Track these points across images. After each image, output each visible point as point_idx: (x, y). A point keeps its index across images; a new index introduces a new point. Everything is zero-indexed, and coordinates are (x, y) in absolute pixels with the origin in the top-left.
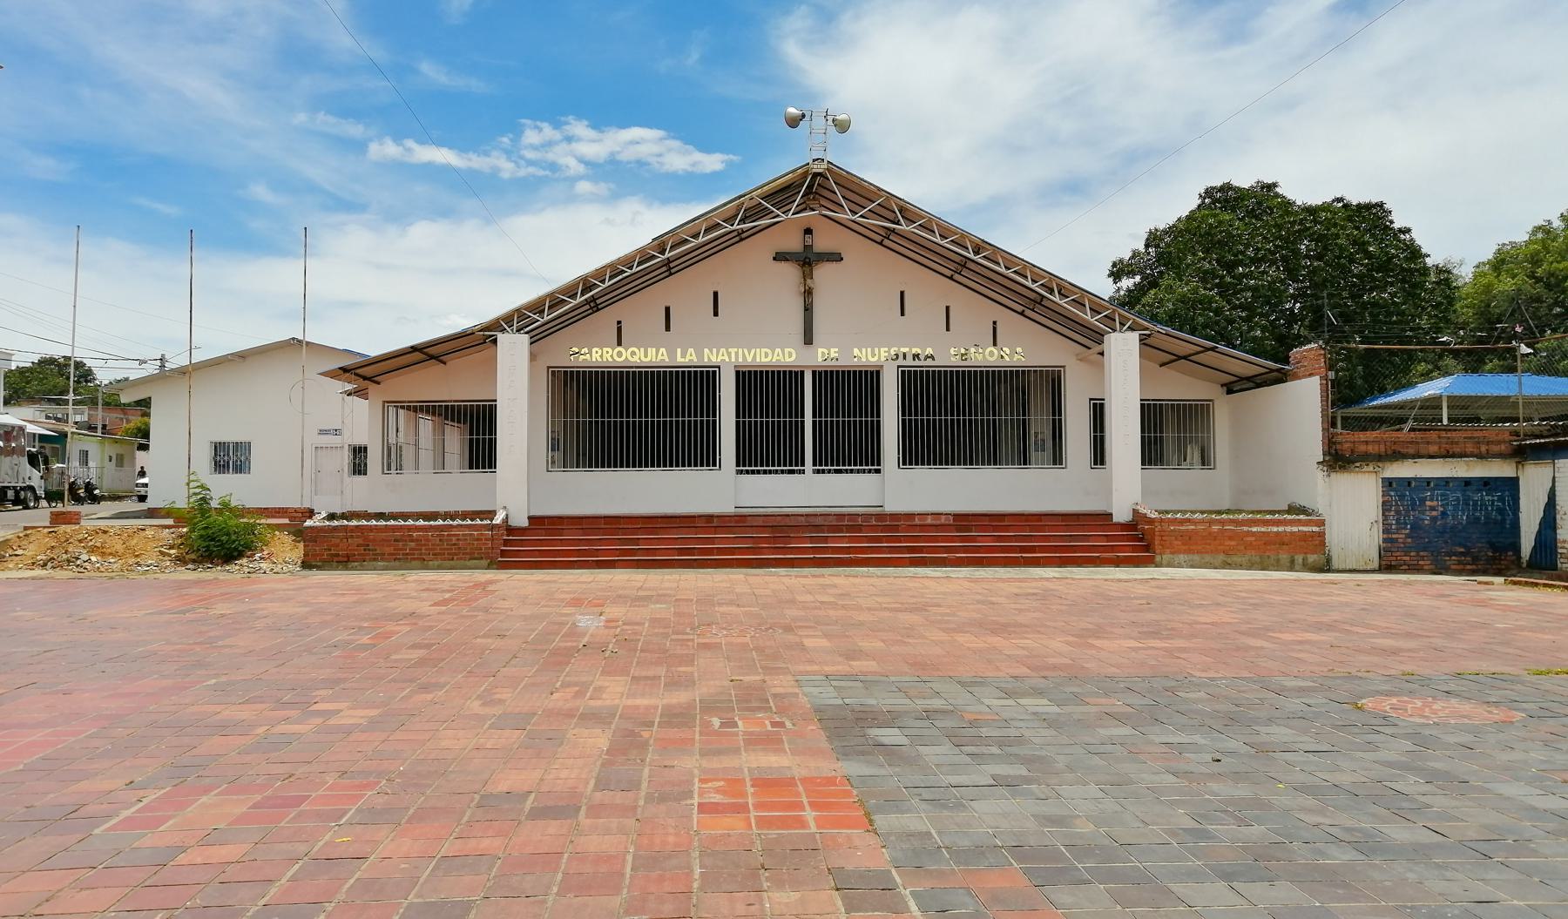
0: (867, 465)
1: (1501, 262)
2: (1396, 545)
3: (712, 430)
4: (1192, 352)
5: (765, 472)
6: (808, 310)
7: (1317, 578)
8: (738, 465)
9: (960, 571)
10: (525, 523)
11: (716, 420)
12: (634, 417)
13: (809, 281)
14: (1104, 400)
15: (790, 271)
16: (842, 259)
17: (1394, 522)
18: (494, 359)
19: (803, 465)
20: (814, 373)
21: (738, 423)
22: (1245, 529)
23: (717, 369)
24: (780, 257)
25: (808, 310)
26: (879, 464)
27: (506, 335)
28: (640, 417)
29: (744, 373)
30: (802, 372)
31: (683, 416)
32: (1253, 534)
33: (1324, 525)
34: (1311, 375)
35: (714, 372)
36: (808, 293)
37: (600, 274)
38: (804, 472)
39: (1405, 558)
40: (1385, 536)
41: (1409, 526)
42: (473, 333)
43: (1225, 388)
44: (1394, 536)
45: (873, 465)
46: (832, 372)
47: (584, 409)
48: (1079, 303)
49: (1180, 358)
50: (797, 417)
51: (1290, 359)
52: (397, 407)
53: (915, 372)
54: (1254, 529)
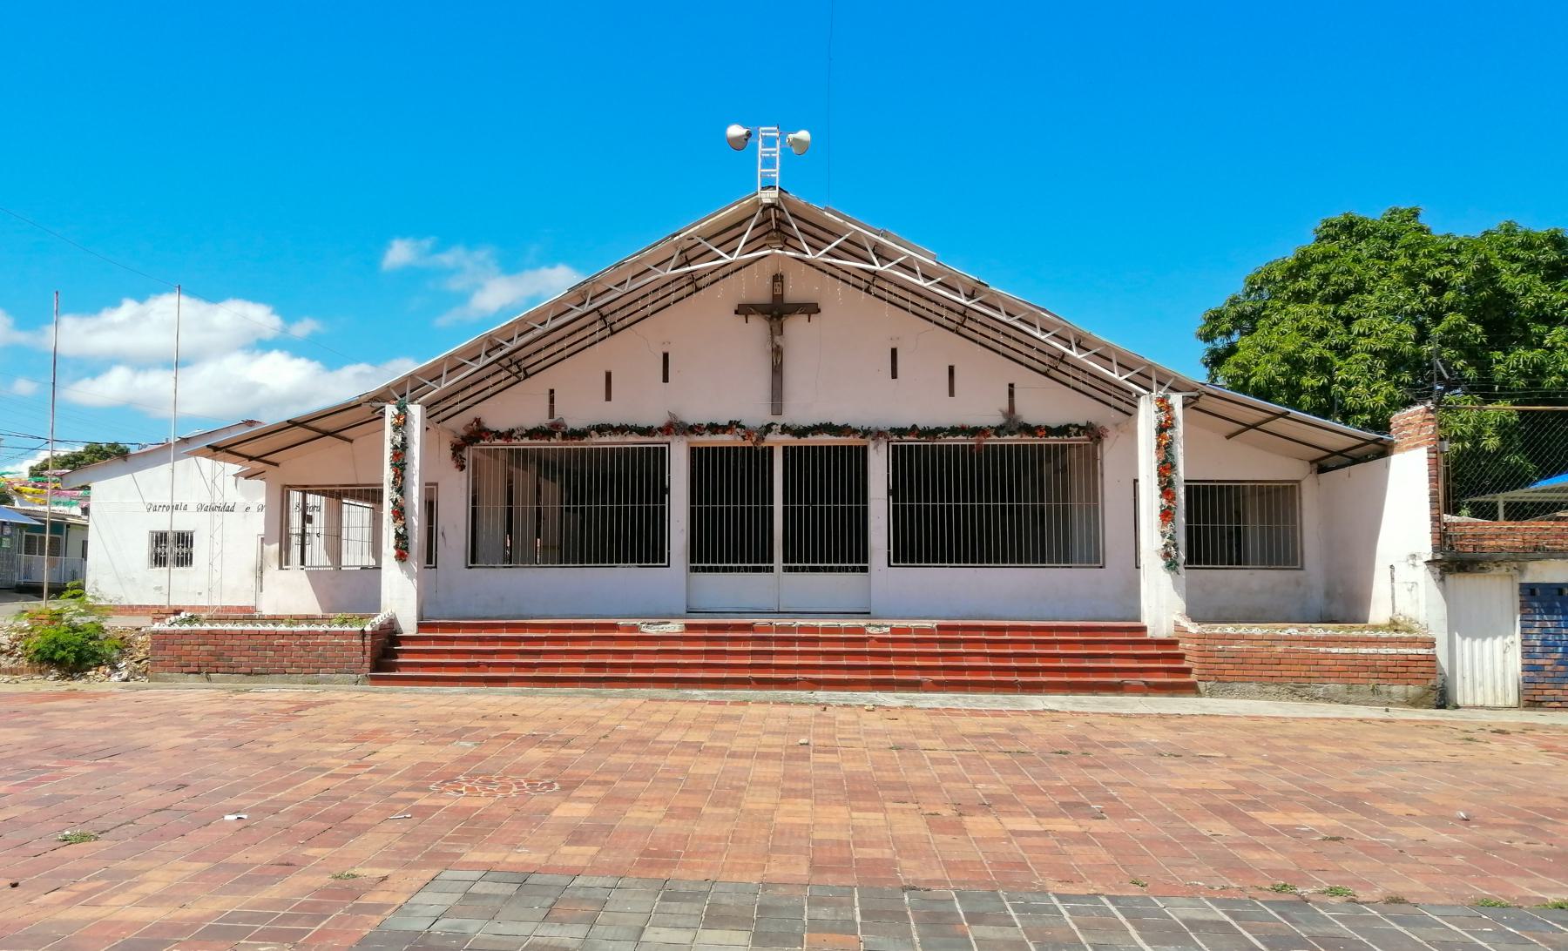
1: (390, 247)
2: (1542, 674)
3: (658, 520)
4: (1262, 419)
5: (725, 570)
6: (777, 370)
7: (1141, 709)
8: (692, 561)
9: (933, 699)
11: (473, 504)
12: (957, 507)
13: (777, 338)
15: (758, 325)
16: (819, 311)
17: (1538, 643)
18: (1387, 466)
19: (771, 561)
21: (692, 510)
22: (1322, 649)
23: (667, 446)
24: (744, 310)
25: (777, 370)
26: (866, 560)
28: (980, 507)
29: (700, 450)
32: (1335, 657)
33: (1434, 645)
34: (1416, 446)
36: (777, 352)
38: (771, 570)
39: (1555, 692)
40: (1526, 661)
41: (1560, 649)
42: (360, 405)
43: (1315, 466)
44: (1539, 662)
48: (1104, 358)
49: (1249, 427)
50: (857, 502)
51: (1392, 426)
52: (305, 491)
54: (1334, 650)
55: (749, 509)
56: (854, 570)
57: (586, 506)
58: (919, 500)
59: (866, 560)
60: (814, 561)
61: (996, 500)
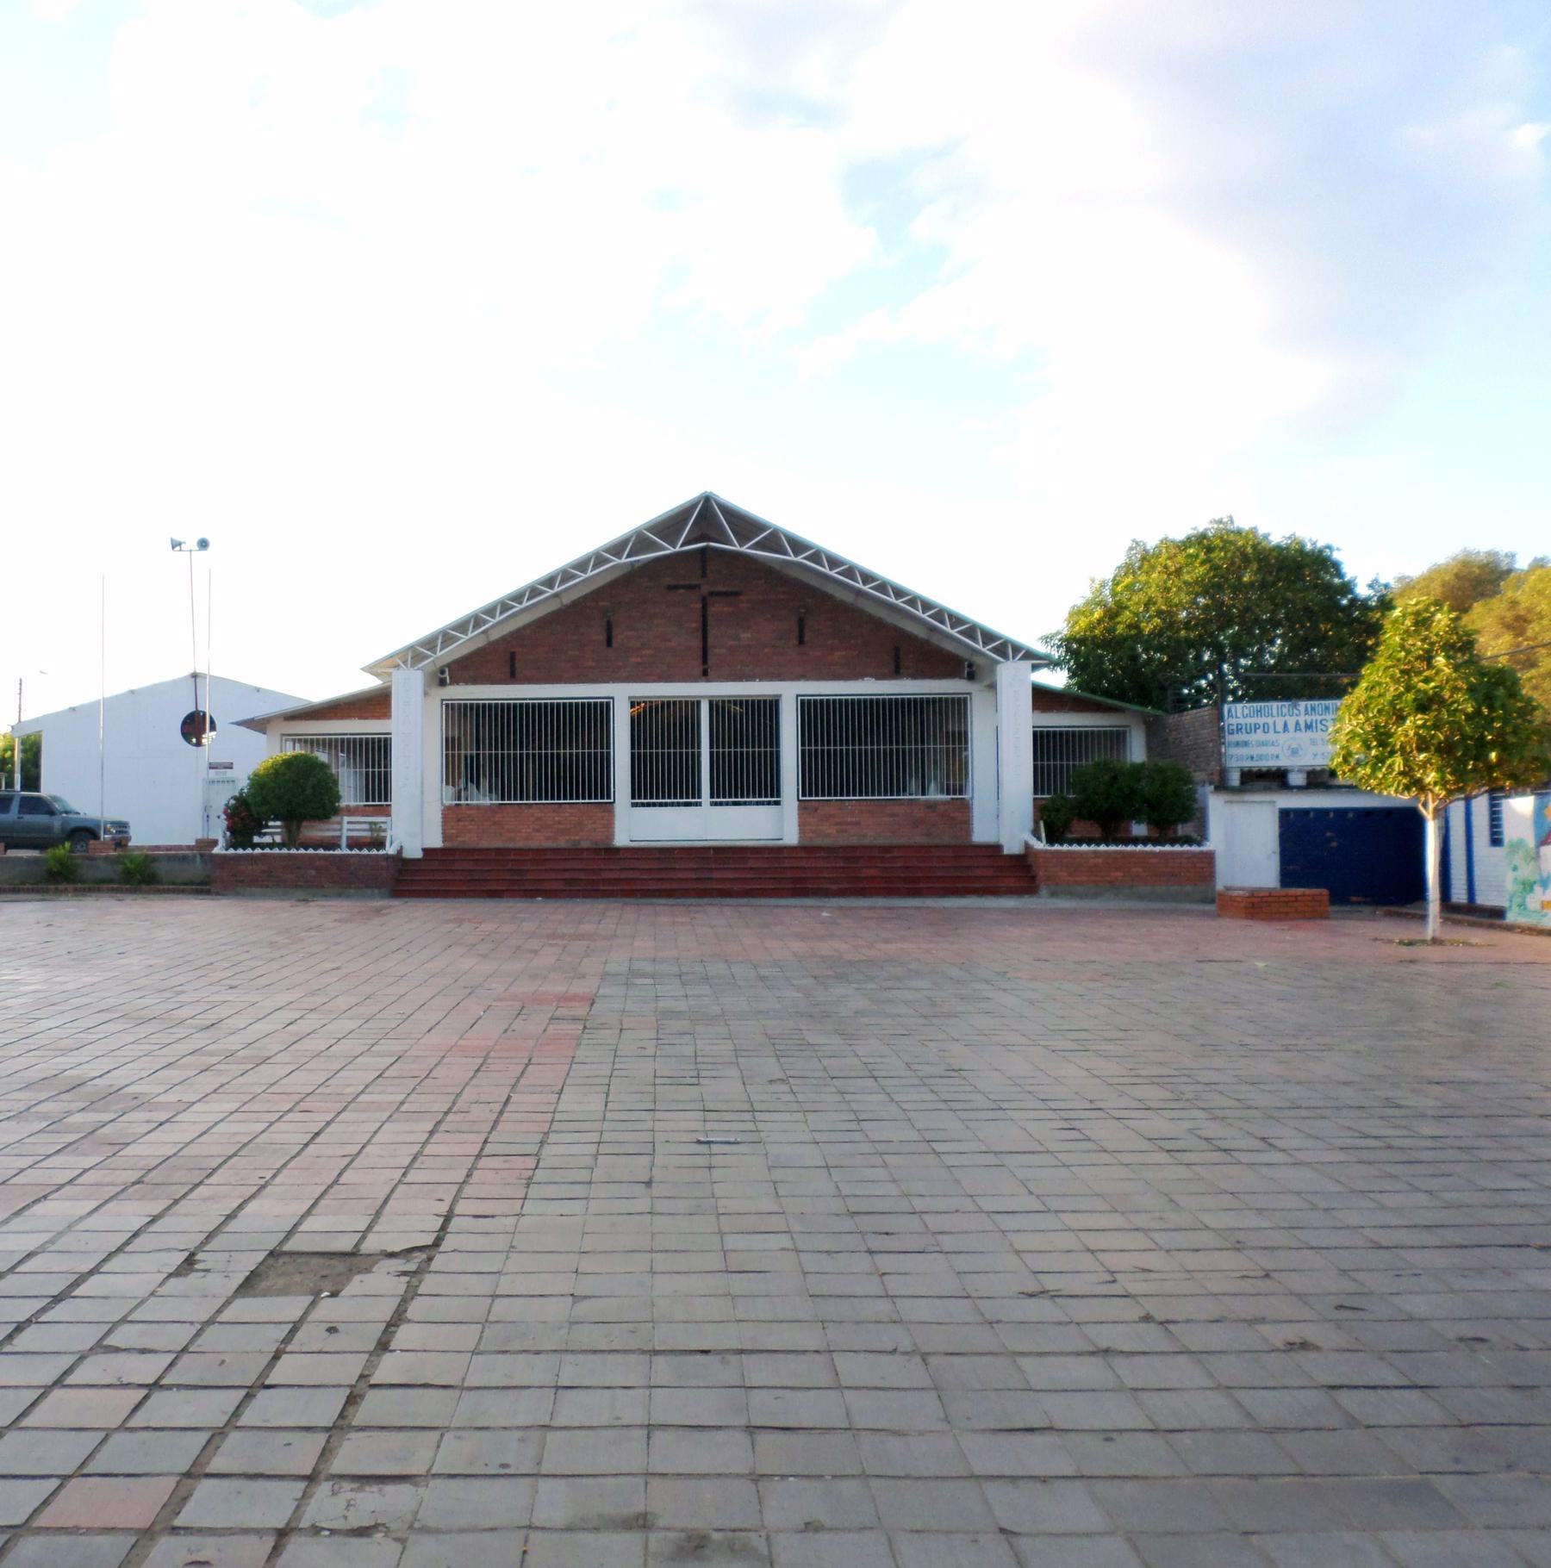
0: (766, 796)
3: (604, 763)
5: (661, 805)
8: (633, 797)
10: (419, 855)
14: (390, 734)
19: (699, 797)
20: (711, 703)
21: (633, 755)
26: (778, 796)
27: (401, 671)
30: (699, 703)
31: (583, 754)
35: (608, 704)
37: (490, 611)
45: (772, 796)
46: (687, 702)
47: (596, 741)
53: (571, 704)
55: (521, 755)
56: (769, 803)
57: (733, 750)
58: (822, 745)
59: (778, 795)
60: (736, 796)
61: (841, 745)
